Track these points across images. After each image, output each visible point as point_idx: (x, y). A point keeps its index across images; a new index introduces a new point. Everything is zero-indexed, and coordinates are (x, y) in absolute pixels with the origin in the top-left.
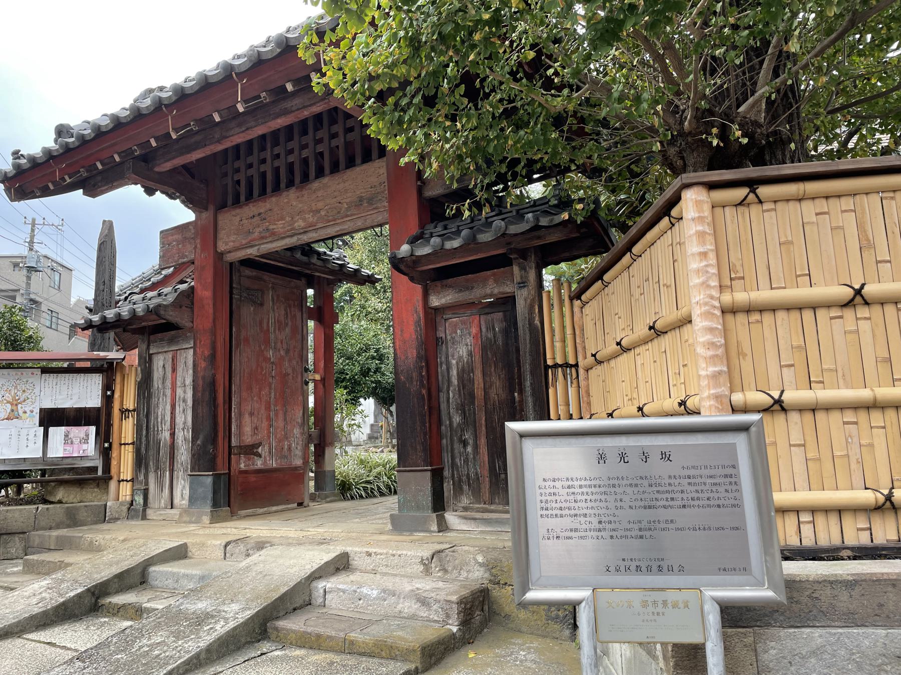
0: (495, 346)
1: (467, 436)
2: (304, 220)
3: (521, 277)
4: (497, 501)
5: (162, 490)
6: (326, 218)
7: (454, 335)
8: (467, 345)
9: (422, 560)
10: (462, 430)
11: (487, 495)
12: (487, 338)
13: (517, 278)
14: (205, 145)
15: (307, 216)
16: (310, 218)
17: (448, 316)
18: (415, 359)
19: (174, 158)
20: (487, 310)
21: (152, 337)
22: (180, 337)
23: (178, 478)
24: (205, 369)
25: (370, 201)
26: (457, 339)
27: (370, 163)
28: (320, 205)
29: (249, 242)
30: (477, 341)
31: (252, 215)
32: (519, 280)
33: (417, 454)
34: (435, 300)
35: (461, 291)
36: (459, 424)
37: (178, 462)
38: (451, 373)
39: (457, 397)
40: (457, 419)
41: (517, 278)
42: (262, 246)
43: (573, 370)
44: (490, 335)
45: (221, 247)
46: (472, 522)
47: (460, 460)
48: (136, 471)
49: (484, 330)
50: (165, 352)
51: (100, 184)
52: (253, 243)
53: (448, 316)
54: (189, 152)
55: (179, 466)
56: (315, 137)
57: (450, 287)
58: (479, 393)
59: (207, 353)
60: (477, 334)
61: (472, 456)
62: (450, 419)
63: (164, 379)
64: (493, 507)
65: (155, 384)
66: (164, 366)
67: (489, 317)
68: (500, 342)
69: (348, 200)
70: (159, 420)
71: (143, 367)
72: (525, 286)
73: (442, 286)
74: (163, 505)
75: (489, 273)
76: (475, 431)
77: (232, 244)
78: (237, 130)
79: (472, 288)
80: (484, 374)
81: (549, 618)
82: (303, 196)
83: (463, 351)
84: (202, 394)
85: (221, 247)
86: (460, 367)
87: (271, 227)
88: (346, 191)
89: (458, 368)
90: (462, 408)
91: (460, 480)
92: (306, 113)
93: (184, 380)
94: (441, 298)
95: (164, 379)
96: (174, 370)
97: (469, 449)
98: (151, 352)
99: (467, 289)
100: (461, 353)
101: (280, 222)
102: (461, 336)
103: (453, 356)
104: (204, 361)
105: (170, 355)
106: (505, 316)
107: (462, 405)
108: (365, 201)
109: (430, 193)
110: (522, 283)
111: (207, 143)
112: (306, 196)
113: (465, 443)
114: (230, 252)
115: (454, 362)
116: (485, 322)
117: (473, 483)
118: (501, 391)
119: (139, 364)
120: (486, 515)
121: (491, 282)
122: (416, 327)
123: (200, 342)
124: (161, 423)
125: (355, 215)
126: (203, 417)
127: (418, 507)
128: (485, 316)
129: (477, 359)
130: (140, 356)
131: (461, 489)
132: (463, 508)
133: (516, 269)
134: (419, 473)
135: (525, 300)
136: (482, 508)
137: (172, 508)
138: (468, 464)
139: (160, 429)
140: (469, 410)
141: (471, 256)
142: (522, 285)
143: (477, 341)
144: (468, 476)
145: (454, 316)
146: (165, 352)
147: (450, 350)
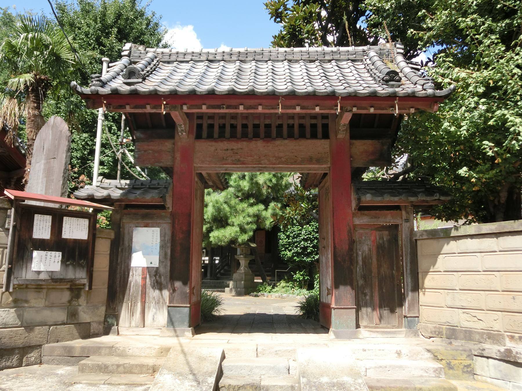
1: (367, 291)
3: (407, 217)
5: (133, 315)
8: (368, 245)
9: (397, 351)
12: (380, 243)
13: (404, 217)
23: (149, 308)
28: (281, 154)
31: (226, 148)
32: (405, 218)
35: (372, 218)
36: (362, 285)
37: (149, 297)
38: (358, 259)
39: (361, 270)
41: (404, 217)
44: (381, 242)
49: (378, 238)
55: (151, 299)
57: (366, 215)
58: (375, 270)
61: (369, 301)
62: (357, 282)
67: (381, 233)
68: (386, 246)
73: (361, 214)
75: (388, 212)
79: (379, 218)
80: (378, 260)
81: (464, 372)
82: (268, 146)
83: (366, 248)
97: (368, 297)
100: (364, 249)
101: (250, 158)
103: (360, 250)
113: (365, 295)
115: (360, 253)
133: (404, 212)
135: (408, 228)
137: (144, 327)
147: (358, 247)
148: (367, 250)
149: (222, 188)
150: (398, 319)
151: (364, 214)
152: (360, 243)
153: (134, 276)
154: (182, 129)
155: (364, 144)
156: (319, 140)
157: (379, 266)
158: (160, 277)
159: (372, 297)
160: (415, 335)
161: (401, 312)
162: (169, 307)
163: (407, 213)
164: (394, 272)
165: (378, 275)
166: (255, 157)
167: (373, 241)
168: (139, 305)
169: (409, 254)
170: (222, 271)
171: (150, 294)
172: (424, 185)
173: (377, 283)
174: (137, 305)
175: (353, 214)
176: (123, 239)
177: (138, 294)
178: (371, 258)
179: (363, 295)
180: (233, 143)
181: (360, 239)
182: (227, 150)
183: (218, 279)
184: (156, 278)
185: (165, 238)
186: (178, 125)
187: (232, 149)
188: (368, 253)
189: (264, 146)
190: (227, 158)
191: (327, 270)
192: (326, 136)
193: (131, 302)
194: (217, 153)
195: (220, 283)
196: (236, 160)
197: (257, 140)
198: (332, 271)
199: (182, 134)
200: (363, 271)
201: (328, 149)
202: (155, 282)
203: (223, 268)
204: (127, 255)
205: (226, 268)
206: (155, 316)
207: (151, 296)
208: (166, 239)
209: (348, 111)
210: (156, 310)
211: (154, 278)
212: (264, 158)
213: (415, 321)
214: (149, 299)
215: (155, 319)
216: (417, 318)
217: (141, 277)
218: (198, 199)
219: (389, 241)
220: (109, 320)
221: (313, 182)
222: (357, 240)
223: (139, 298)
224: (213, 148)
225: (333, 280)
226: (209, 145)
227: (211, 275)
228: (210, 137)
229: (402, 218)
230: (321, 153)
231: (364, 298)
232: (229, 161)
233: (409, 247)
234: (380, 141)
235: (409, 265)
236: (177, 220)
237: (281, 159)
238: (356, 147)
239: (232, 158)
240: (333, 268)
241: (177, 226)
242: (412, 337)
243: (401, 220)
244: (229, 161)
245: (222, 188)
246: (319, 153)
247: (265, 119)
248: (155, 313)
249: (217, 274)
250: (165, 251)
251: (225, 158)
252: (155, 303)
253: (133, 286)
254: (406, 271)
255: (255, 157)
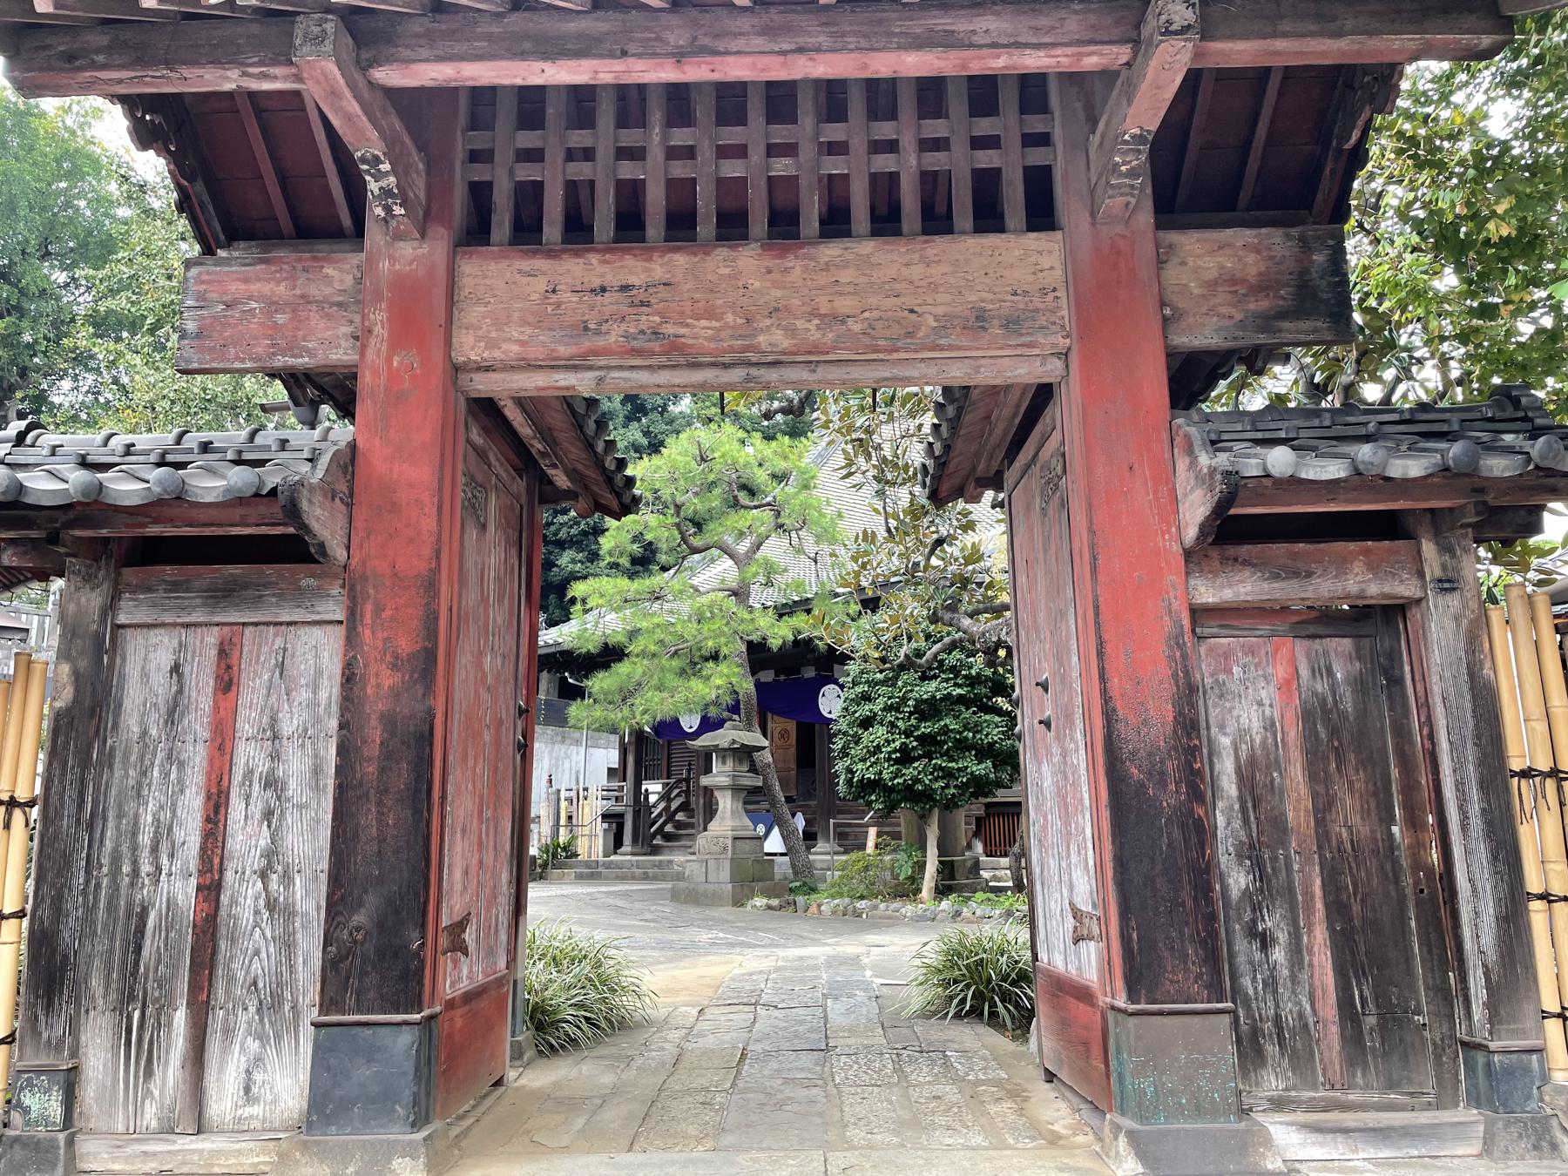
0: (1335, 716)
1: (1272, 921)
2: (791, 332)
3: (1444, 567)
4: (1359, 1080)
5: (149, 1073)
6: (866, 340)
7: (1222, 677)
8: (1260, 704)
10: (1256, 908)
11: (1337, 1067)
12: (1315, 693)
14: (624, 53)
15: (800, 324)
16: (812, 331)
17: (1207, 631)
18: (1169, 729)
19: (462, 58)
20: (1312, 630)
21: (129, 574)
22: (266, 586)
23: (228, 1032)
24: (396, 694)
25: (1012, 324)
26: (1233, 687)
27: (1049, 233)
28: (845, 305)
29: (583, 357)
30: (1290, 696)
31: (596, 283)
32: (1438, 573)
33: (1187, 970)
34: (1203, 589)
35: (1277, 577)
36: (1246, 893)
37: (231, 979)
38: (1217, 767)
39: (1237, 824)
40: (1238, 880)
42: (615, 374)
43: (1550, 784)
44: (1321, 687)
45: (468, 348)
46: (1340, 1138)
47: (1254, 979)
48: (31, 1006)
49: (1305, 673)
50: (187, 626)
51: (100, 58)
52: (593, 360)
53: (1207, 631)
54: (548, 56)
56: (817, 134)
57: (1246, 563)
59: (406, 645)
60: (1288, 682)
61: (1286, 972)
63: (174, 711)
64: (1353, 1097)
65: (131, 722)
66: (176, 669)
67: (1317, 645)
68: (1348, 705)
69: (940, 310)
70: (145, 838)
71: (83, 664)
72: (1454, 589)
74: (150, 1115)
75: (1352, 546)
76: (1293, 908)
77: (515, 348)
78: (758, 42)
79: (1309, 575)
82: (786, 270)
84: (382, 771)
85: (468, 348)
86: (1244, 755)
87: (669, 329)
88: (933, 287)
89: (1237, 757)
90: (1251, 854)
91: (1255, 1033)
92: (998, 63)
93: (274, 720)
94: (1222, 586)
95: (174, 711)
96: (227, 683)
97: (1278, 955)
98: (122, 619)
99: (1295, 574)
100: (1244, 720)
101: (704, 323)
102: (1243, 681)
103: (1222, 727)
104: (394, 667)
105: (211, 638)
106: (1358, 649)
107: (1252, 846)
108: (995, 322)
109: (1185, 340)
110: (1448, 581)
111: (632, 48)
112: (798, 271)
113: (1266, 941)
114: (487, 369)
115: (1225, 741)
116: (1308, 656)
117: (1293, 1037)
118: (1355, 820)
119: (64, 654)
120: (1350, 1119)
121: (1358, 567)
122: (1170, 647)
123: (378, 610)
124: (155, 849)
125: (959, 348)
126: (381, 840)
127: (1198, 1108)
128: (1306, 642)
129: (1293, 734)
130: (70, 630)
131: (1260, 1054)
132: (1271, 1100)
133: (1428, 548)
134: (1197, 1019)
135: (1457, 619)
136: (1323, 1099)
138: (1275, 991)
139: (146, 868)
140: (1274, 859)
141: (1376, 501)
142: (1446, 585)
143: (1290, 696)
144: (1277, 1020)
145: (1224, 632)
146: (187, 626)
148: (1256, 725)
149: (614, 504)
150: (1438, 1057)
151: (1236, 560)
152: (1221, 696)
153: (163, 877)
154: (383, 183)
155: (1220, 248)
156: (1012, 237)
157: (1323, 808)
158: (287, 879)
159: (1296, 950)
160: (1536, 1147)
161: (1445, 1027)
162: (316, 1025)
163: (1446, 549)
164: (1395, 829)
165: (1320, 847)
166: (730, 318)
167: (1285, 687)
168: (180, 1018)
169: (1469, 745)
170: (669, 828)
171: (235, 966)
172: (1521, 414)
173: (1318, 882)
174: (170, 1024)
175: (1188, 554)
176: (119, 704)
177: (175, 967)
178: (1275, 764)
179: (1256, 945)
180: (629, 261)
181: (1222, 677)
182: (603, 289)
183: (655, 850)
184: (266, 889)
185: (315, 693)
186: (364, 160)
187: (625, 288)
188: (1264, 742)
189: (769, 272)
190: (604, 328)
191: (1067, 823)
192: (1041, 215)
193: (144, 1006)
194: (558, 305)
195: (660, 865)
196: (642, 332)
197: (737, 246)
198: (1096, 825)
199: (388, 209)
200: (1246, 821)
201: (1059, 272)
202: (262, 902)
203: (671, 818)
204: (131, 782)
205: (680, 816)
206: (258, 1077)
207: (240, 975)
208: (323, 695)
209: (1176, 33)
210: (263, 1046)
211: (259, 884)
212: (768, 322)
213: (1527, 1070)
214: (228, 992)
215: (255, 1090)
216: (1534, 1057)
217: (193, 881)
218: (491, 527)
219: (1360, 685)
220: (28, 1100)
221: (974, 469)
222: (1208, 681)
223: (183, 985)
224: (541, 284)
225: (1110, 873)
226: (520, 271)
227: (635, 841)
228: (527, 232)
229: (1421, 574)
230: (1026, 292)
231: (1258, 956)
232: (612, 338)
233: (1468, 706)
234: (1295, 231)
235: (1474, 794)
236: (369, 609)
237: (843, 322)
238: (1183, 263)
239: (624, 326)
240: (1106, 814)
241: (368, 632)
242: (1522, 1158)
243: (1415, 582)
244: (612, 338)
245: (614, 504)
246: (1015, 294)
247: (769, 155)
248: (258, 1060)
249: (654, 836)
250: (316, 756)
251: (592, 326)
252: (259, 1011)
253: (157, 927)
254: (1464, 827)
255: (730, 318)
